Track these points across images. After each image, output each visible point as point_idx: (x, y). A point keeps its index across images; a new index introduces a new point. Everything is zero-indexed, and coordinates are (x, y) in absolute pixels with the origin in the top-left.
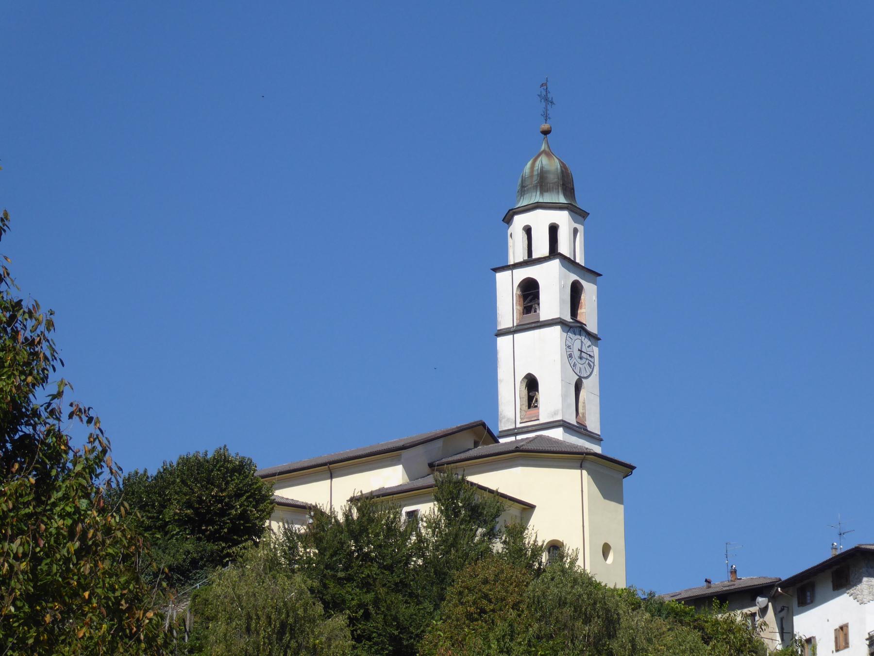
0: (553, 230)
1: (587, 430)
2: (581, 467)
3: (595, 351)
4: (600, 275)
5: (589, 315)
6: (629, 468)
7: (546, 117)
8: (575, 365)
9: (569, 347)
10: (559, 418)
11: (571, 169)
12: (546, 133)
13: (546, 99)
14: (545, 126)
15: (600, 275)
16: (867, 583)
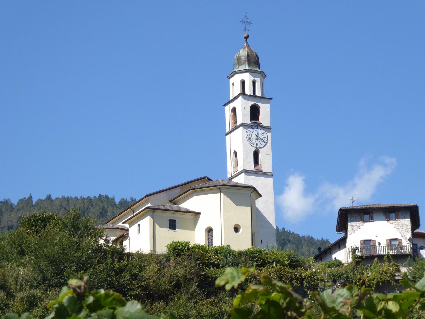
0: (243, 83)
1: (263, 172)
2: (220, 192)
3: (269, 135)
4: (271, 99)
5: (265, 117)
6: (260, 196)
7: (246, 30)
8: (253, 143)
9: (249, 135)
10: (243, 169)
11: (32, 195)
12: (246, 38)
13: (246, 22)
14: (245, 35)
15: (271, 99)
16: (2, 200)
